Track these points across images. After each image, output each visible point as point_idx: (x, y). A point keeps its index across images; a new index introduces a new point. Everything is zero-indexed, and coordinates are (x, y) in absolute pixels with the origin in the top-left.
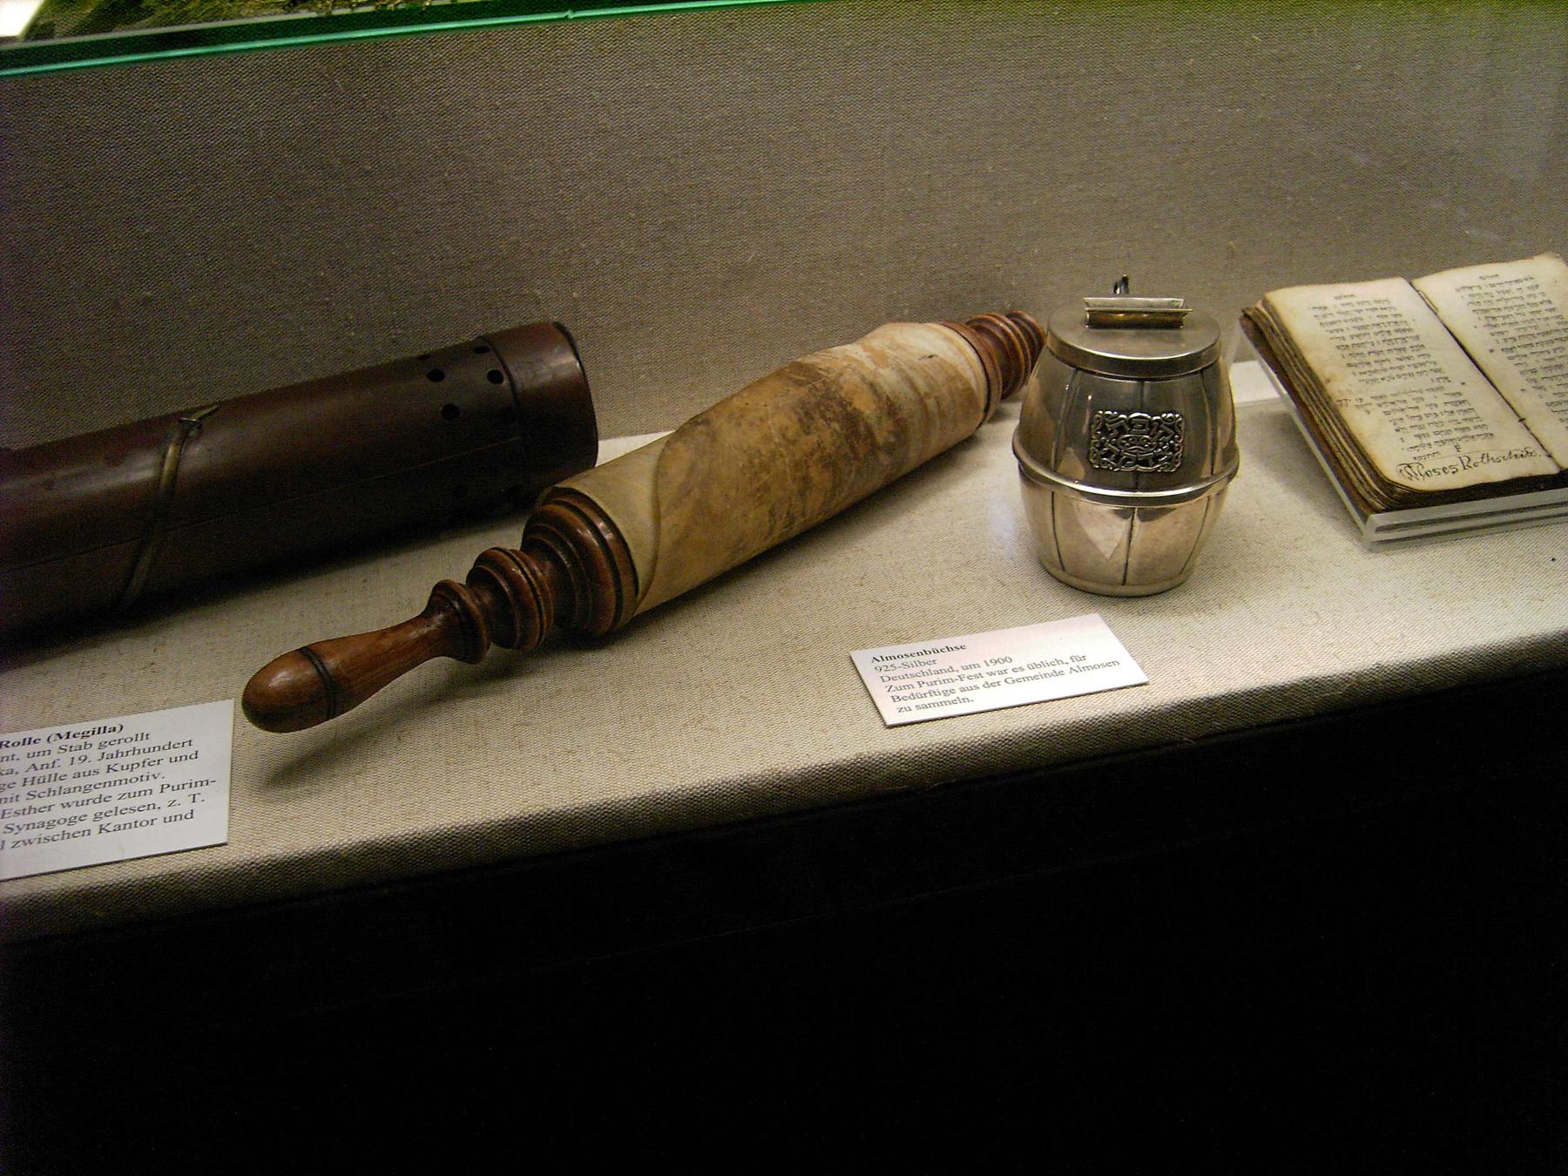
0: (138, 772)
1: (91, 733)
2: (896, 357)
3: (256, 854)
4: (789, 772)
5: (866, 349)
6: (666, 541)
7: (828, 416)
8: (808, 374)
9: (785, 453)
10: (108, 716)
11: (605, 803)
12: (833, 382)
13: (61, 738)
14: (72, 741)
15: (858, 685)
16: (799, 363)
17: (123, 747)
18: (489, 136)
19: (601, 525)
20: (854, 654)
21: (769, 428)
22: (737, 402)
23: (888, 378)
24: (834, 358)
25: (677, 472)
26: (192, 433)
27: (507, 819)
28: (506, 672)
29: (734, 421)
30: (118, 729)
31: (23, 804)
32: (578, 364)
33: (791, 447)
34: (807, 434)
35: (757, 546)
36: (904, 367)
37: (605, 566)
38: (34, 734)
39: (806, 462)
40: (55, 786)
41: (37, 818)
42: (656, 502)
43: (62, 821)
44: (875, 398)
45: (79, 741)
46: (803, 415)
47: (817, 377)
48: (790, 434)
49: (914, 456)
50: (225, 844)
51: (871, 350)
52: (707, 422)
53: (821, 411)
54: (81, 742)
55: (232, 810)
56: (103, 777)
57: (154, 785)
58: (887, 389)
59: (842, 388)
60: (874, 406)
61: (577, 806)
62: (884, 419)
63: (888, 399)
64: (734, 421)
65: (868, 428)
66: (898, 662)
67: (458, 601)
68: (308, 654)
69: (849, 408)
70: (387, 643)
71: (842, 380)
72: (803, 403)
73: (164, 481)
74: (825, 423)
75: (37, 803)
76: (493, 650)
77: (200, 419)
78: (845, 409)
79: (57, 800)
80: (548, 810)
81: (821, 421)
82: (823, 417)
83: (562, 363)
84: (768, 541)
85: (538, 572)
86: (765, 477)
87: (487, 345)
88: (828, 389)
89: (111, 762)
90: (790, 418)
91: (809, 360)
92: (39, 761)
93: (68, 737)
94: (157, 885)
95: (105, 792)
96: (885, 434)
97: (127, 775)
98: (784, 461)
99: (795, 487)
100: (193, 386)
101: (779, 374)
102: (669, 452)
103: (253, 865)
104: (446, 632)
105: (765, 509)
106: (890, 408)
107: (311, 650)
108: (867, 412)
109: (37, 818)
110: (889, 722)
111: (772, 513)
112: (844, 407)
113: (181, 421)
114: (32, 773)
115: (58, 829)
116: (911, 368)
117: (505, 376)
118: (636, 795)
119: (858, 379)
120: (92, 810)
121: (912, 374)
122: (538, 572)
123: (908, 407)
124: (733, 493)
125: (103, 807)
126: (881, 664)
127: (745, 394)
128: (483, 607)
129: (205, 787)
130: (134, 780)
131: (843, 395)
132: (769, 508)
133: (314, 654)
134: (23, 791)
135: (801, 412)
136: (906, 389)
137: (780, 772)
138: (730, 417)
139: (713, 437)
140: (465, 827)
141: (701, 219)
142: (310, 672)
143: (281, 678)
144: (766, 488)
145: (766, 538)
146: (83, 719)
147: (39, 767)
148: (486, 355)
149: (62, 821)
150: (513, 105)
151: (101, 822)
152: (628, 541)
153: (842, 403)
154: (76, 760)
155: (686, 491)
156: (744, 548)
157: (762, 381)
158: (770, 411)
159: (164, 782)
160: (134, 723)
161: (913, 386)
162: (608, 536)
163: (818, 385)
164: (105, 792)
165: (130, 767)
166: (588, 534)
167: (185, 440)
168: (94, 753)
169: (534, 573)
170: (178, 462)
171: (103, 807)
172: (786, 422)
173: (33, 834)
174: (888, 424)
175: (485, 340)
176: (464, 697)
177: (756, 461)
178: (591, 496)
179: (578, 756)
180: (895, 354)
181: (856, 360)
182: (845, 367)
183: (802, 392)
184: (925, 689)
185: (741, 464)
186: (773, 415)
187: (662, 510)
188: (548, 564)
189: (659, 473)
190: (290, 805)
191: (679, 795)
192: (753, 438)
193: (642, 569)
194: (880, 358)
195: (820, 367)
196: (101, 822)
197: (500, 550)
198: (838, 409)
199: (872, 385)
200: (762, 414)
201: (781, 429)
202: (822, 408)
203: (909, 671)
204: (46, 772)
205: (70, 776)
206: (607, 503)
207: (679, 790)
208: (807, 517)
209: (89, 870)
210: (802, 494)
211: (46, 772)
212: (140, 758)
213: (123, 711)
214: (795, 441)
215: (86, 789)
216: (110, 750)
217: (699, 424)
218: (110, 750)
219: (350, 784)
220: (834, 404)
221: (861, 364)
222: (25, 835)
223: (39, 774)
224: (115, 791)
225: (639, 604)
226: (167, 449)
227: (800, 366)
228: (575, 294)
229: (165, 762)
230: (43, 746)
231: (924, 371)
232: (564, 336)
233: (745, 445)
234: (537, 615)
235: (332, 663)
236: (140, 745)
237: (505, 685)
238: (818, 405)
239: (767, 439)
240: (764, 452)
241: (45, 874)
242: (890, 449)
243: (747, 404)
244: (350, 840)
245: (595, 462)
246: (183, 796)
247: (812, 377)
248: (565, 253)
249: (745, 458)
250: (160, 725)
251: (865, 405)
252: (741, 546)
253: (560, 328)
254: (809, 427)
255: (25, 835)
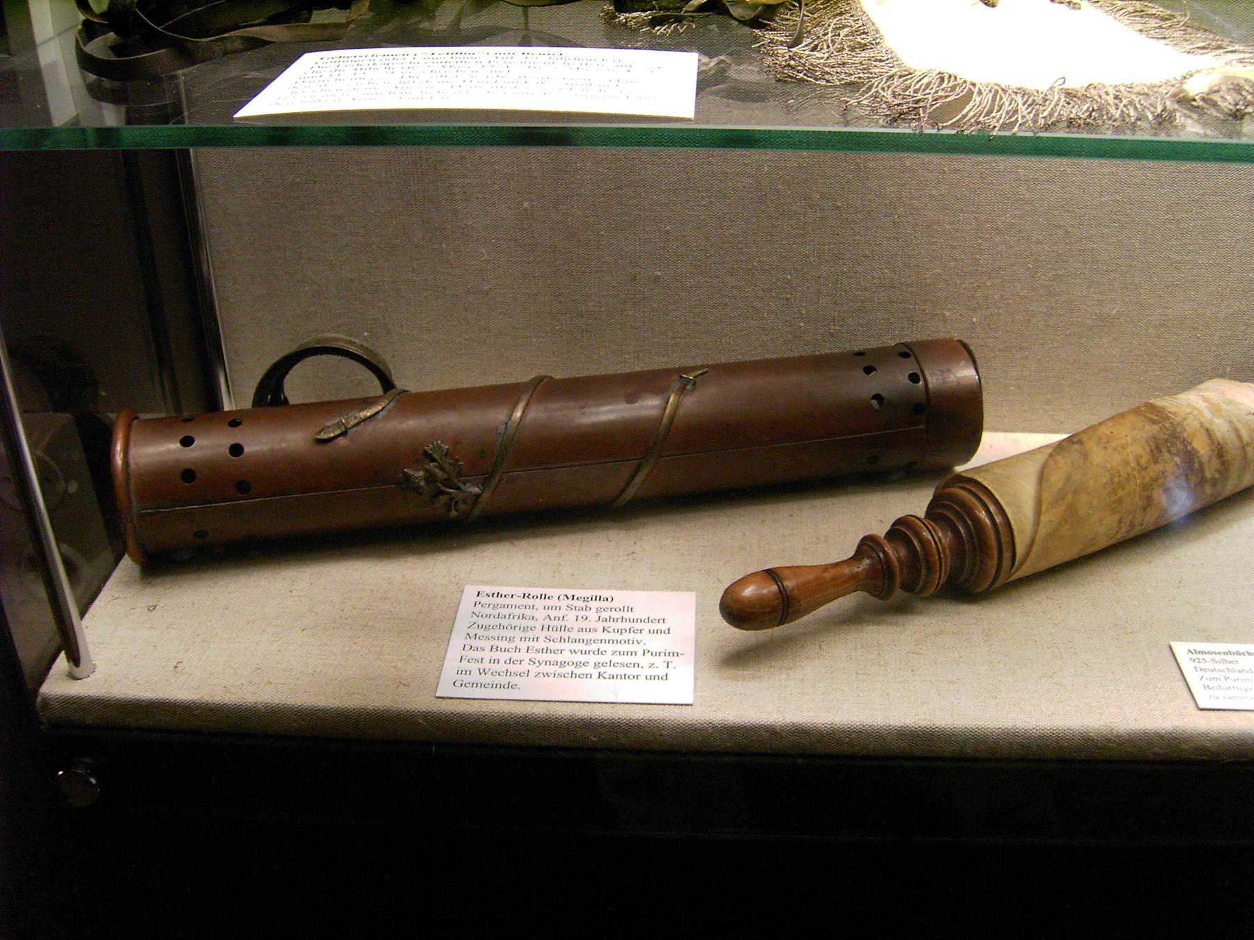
0: (626, 636)
1: (590, 599)
2: (1228, 411)
3: (713, 717)
4: (1120, 730)
5: (1206, 400)
6: (1042, 531)
7: (1172, 451)
8: (1156, 415)
9: (1137, 476)
10: (602, 588)
11: (977, 728)
12: (1178, 424)
13: (568, 598)
14: (575, 603)
15: (1176, 670)
16: (1152, 404)
17: (615, 615)
18: (934, 192)
19: (992, 508)
20: (1175, 645)
21: (1128, 454)
22: (1104, 430)
23: (1221, 427)
24: (1180, 404)
25: (1056, 479)
26: (688, 387)
27: (902, 726)
28: (903, 609)
29: (1102, 445)
30: (610, 599)
31: (541, 644)
32: (977, 377)
33: (1143, 472)
34: (1156, 463)
35: (1103, 543)
36: (1235, 420)
37: (994, 544)
38: (549, 592)
39: (1152, 485)
40: (565, 635)
41: (552, 657)
42: (1039, 502)
43: (571, 664)
44: (1209, 442)
45: (580, 604)
46: (1154, 448)
47: (1167, 418)
48: (1143, 461)
49: (1230, 487)
50: (691, 705)
51: (1206, 400)
52: (1080, 442)
53: (1167, 447)
54: (583, 605)
55: (696, 679)
56: (600, 635)
57: (639, 648)
58: (1219, 435)
59: (1185, 430)
60: (1207, 448)
61: (955, 726)
62: (1214, 459)
63: (1219, 444)
64: (1102, 445)
65: (1201, 465)
66: (1208, 657)
67: (883, 553)
68: (772, 574)
69: (1189, 448)
70: (827, 575)
71: (1185, 423)
72: (1155, 438)
73: (665, 420)
74: (1169, 456)
75: (552, 646)
76: (899, 593)
77: (695, 377)
78: (1186, 447)
79: (568, 646)
80: (934, 725)
81: (1168, 454)
82: (1169, 451)
83: (965, 374)
84: (1113, 540)
85: (938, 538)
86: (1121, 493)
87: (908, 351)
88: (1175, 429)
89: (607, 624)
90: (1145, 449)
91: (1160, 403)
92: (553, 613)
93: (573, 599)
94: (639, 726)
95: (603, 647)
96: (1213, 471)
97: (617, 636)
98: (1136, 482)
99: (1141, 504)
100: (676, 345)
101: (1136, 411)
102: (1051, 463)
103: (710, 725)
104: (872, 573)
105: (1116, 517)
106: (1220, 451)
107: (773, 571)
108: (1202, 452)
109: (552, 657)
110: (1201, 706)
111: (1120, 521)
112: (1186, 446)
113: (681, 377)
114: (547, 622)
115: (568, 669)
116: (1238, 421)
117: (921, 378)
118: (1000, 726)
119: (1198, 425)
120: (592, 659)
121: (1239, 425)
122: (938, 538)
123: (1233, 452)
124: (1095, 502)
125: (600, 658)
126: (1195, 656)
127: (1110, 424)
128: (899, 559)
129: (675, 657)
130: (623, 642)
131: (1186, 436)
132: (1119, 517)
133: (778, 576)
134: (542, 635)
135: (1153, 445)
136: (1234, 438)
137: (1113, 729)
138: (1099, 440)
139: (1085, 455)
140: (870, 726)
141: (1082, 276)
142: (774, 588)
143: (748, 591)
144: (1120, 501)
145: (1112, 538)
146: (583, 587)
147: (553, 619)
148: (908, 360)
149: (571, 664)
150: (957, 171)
151: (599, 670)
152: (1014, 527)
153: (1185, 442)
154: (580, 618)
155: (1061, 496)
156: (1093, 545)
157: (1122, 415)
158: (1130, 442)
159: (645, 647)
160: (623, 597)
161: (1239, 436)
162: (998, 520)
163: (1167, 425)
164: (603, 647)
165: (620, 631)
166: (983, 515)
167: (682, 391)
168: (593, 615)
169: (940, 540)
170: (677, 407)
171: (600, 658)
172: (1140, 451)
173: (550, 669)
174: (1215, 463)
175: (906, 346)
176: (869, 622)
177: (1116, 480)
178: (990, 488)
179: (957, 685)
180: (1228, 408)
181: (1196, 409)
182: (1188, 414)
183: (1155, 428)
184: (1230, 683)
185: (1104, 481)
186: (1131, 445)
187: (1043, 507)
188: (949, 534)
189: (1042, 478)
190: (739, 683)
191: (1033, 732)
192: (1116, 460)
193: (1020, 550)
194: (1216, 410)
195: (1170, 410)
196: (599, 670)
197: (911, 516)
198: (1180, 447)
199: (1207, 430)
200: (1123, 442)
201: (1137, 456)
202: (1169, 444)
203: (1218, 666)
204: (557, 623)
205: (576, 629)
206: (1001, 495)
207: (1034, 728)
208: (1143, 526)
209: (591, 705)
210: (1144, 509)
211: (557, 623)
212: (627, 626)
213: (612, 586)
214: (1147, 468)
215: (588, 642)
216: (605, 615)
217: (1074, 443)
218: (605, 615)
219: (784, 676)
220: (1178, 443)
221: (1201, 412)
222: (543, 668)
223: (553, 623)
224: (609, 648)
225: (1012, 575)
226: (670, 397)
227: (1152, 407)
228: (974, 320)
229: (645, 632)
230: (554, 602)
231: (1249, 425)
232: (965, 351)
233: (1109, 465)
234: (938, 573)
235: (789, 584)
236: (627, 615)
237: (901, 619)
238: (1166, 441)
239: (1126, 463)
240: (1122, 474)
241: (558, 702)
242: (1214, 482)
243: (1112, 432)
244: (784, 720)
245: (236, 113)
246: (659, 661)
247: (1162, 418)
248: (973, 287)
249: (1109, 476)
250: (643, 602)
251: (1201, 447)
252: (1092, 543)
253: (965, 346)
254: (1157, 458)
255: (543, 668)
